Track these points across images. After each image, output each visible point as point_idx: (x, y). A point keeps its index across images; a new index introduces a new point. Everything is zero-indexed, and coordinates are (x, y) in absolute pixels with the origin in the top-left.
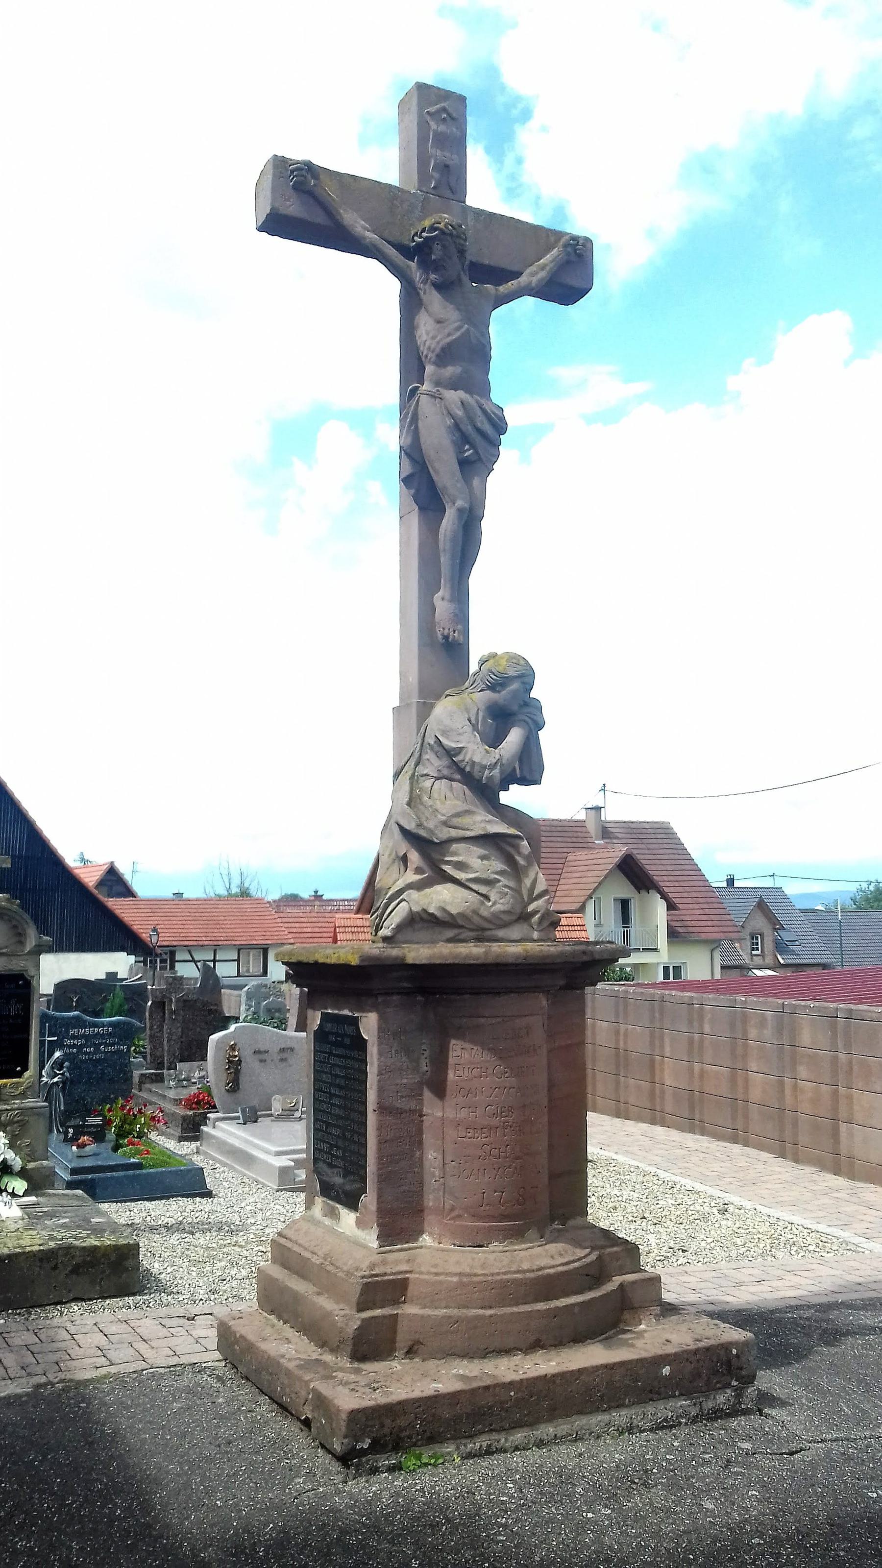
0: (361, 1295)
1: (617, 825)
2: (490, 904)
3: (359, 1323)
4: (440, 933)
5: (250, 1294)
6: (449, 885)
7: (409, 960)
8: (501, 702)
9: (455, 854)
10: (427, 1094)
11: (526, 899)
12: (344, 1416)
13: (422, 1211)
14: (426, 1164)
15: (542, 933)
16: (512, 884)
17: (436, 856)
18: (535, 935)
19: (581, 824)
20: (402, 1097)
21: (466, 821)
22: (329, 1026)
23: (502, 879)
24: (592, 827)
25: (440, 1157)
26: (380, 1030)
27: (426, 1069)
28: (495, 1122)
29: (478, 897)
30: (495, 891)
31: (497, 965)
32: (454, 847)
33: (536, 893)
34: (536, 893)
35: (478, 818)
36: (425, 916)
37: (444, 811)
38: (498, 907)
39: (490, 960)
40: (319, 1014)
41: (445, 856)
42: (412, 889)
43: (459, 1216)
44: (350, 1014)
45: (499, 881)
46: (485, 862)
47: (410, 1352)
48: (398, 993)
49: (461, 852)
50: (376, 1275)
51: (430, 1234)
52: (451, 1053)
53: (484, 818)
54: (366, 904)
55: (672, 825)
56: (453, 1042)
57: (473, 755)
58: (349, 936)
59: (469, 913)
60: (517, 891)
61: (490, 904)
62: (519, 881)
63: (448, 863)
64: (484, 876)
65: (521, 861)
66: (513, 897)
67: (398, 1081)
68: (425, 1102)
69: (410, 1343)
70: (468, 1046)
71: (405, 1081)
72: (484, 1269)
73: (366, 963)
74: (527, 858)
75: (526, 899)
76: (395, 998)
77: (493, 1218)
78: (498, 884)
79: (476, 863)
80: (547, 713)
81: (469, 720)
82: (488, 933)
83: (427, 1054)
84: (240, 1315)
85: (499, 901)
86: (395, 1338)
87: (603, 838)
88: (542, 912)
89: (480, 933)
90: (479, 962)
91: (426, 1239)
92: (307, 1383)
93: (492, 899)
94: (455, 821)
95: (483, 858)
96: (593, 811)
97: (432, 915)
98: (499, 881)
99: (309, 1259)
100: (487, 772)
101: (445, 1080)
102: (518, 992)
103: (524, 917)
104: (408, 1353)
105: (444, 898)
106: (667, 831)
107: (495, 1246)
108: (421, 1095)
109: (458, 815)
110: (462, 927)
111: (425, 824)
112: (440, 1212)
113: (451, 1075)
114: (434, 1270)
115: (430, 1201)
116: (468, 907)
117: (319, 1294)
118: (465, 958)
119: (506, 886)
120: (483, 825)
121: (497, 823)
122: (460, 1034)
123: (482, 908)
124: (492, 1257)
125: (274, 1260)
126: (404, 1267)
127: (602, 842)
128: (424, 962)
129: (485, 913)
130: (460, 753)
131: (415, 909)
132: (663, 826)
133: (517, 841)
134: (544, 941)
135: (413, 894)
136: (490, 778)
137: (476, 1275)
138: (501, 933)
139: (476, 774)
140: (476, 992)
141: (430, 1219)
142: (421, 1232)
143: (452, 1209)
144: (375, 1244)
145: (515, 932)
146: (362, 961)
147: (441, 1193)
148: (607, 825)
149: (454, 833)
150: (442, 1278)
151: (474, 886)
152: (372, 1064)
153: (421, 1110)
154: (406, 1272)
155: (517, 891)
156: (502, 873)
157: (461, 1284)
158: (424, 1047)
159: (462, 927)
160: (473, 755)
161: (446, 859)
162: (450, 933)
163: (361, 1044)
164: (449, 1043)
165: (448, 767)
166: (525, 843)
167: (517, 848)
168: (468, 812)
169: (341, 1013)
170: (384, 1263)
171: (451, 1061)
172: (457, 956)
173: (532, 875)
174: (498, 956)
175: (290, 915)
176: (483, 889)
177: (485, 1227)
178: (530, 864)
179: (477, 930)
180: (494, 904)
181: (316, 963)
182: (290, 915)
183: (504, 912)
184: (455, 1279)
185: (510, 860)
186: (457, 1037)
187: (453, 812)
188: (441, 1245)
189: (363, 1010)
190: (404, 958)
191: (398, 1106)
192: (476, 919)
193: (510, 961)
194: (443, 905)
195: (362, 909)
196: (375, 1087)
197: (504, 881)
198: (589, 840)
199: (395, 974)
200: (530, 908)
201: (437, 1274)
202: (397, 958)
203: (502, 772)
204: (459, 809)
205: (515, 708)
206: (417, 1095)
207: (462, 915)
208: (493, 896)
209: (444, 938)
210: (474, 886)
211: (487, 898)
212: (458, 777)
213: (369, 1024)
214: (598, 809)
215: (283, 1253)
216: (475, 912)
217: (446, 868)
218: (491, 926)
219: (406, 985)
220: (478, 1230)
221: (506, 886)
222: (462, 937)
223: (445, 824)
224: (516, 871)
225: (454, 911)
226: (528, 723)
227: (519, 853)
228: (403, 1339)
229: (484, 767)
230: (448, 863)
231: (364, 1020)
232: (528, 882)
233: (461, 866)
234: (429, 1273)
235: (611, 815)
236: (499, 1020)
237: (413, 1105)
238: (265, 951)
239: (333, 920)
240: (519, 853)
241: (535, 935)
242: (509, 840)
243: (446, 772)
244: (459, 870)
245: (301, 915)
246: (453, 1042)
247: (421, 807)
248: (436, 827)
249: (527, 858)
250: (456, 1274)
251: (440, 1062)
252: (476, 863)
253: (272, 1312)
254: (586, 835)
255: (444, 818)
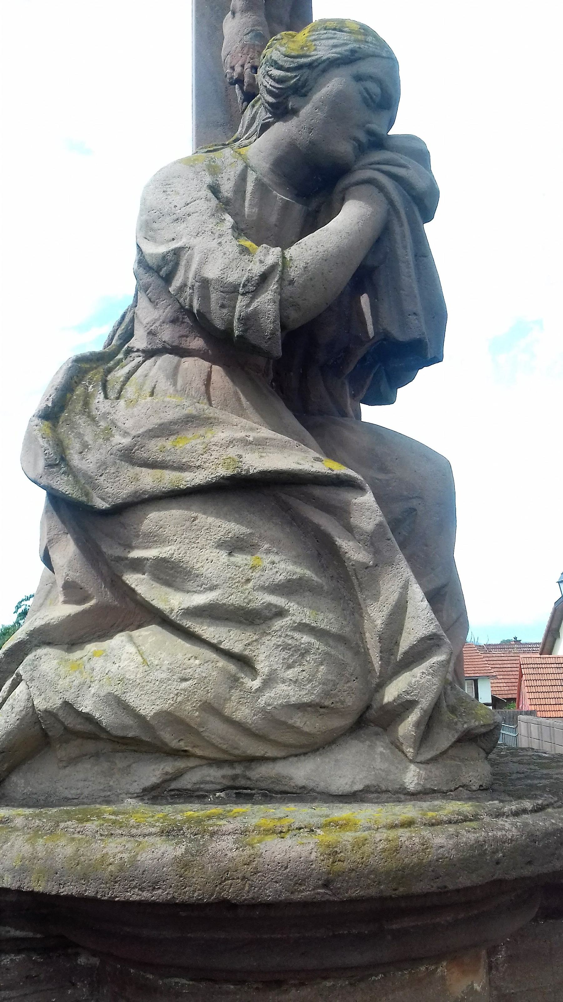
2: (256, 684)
4: (126, 771)
6: (154, 628)
8: (303, 138)
9: (153, 539)
11: (377, 663)
15: (436, 771)
16: (326, 620)
17: (111, 550)
18: (412, 777)
21: (187, 444)
23: (292, 606)
29: (222, 663)
30: (270, 641)
32: (154, 518)
33: (406, 642)
34: (406, 642)
35: (221, 435)
36: (71, 722)
37: (129, 424)
38: (283, 693)
39: (196, 890)
41: (130, 547)
42: (49, 644)
45: (281, 613)
46: (239, 558)
49: (168, 532)
53: (240, 435)
54: (547, 647)
57: (204, 262)
58: (531, 671)
59: (190, 711)
60: (349, 641)
61: (256, 684)
62: (353, 610)
63: (137, 565)
64: (235, 599)
65: (354, 552)
66: (326, 658)
74: (373, 541)
75: (377, 663)
78: (278, 624)
79: (210, 561)
80: (444, 171)
81: (215, 190)
85: (284, 675)
88: (425, 703)
89: (238, 770)
90: (159, 895)
93: (263, 667)
94: (155, 448)
95: (234, 546)
97: (88, 718)
98: (281, 613)
100: (241, 302)
103: (371, 720)
105: (135, 671)
109: (165, 430)
110: (183, 754)
111: (76, 460)
116: (189, 694)
119: (302, 628)
120: (232, 452)
121: (283, 447)
123: (236, 694)
129: (243, 713)
130: (177, 265)
131: (40, 704)
133: (346, 495)
134: (444, 794)
135: (47, 662)
136: (249, 320)
138: (301, 772)
139: (218, 317)
145: (346, 767)
149: (149, 480)
151: (208, 631)
155: (349, 641)
156: (289, 588)
159: (183, 754)
160: (204, 262)
161: (136, 554)
162: (151, 773)
165: (174, 321)
166: (368, 499)
167: (341, 513)
168: (191, 421)
173: (389, 590)
174: (225, 875)
175: (494, 655)
176: (233, 638)
178: (381, 562)
179: (231, 763)
180: (269, 682)
182: (494, 655)
183: (301, 707)
185: (324, 553)
187: (154, 421)
192: (215, 729)
193: (269, 894)
194: (117, 690)
195: (545, 650)
197: (298, 611)
200: (391, 693)
203: (283, 304)
204: (171, 415)
205: (344, 148)
207: (170, 718)
208: (266, 658)
209: (136, 788)
210: (208, 631)
211: (245, 662)
212: (197, 343)
216: (211, 708)
217: (133, 579)
218: (271, 752)
221: (302, 628)
222: (188, 781)
223: (128, 456)
224: (342, 583)
225: (147, 707)
226: (381, 189)
227: (350, 529)
229: (232, 291)
230: (137, 565)
232: (377, 615)
233: (170, 573)
238: (476, 681)
239: (517, 658)
240: (350, 529)
241: (412, 777)
242: (318, 492)
243: (167, 335)
244: (168, 584)
245: (502, 655)
247: (81, 421)
248: (103, 465)
249: (373, 541)
252: (210, 561)
255: (126, 441)
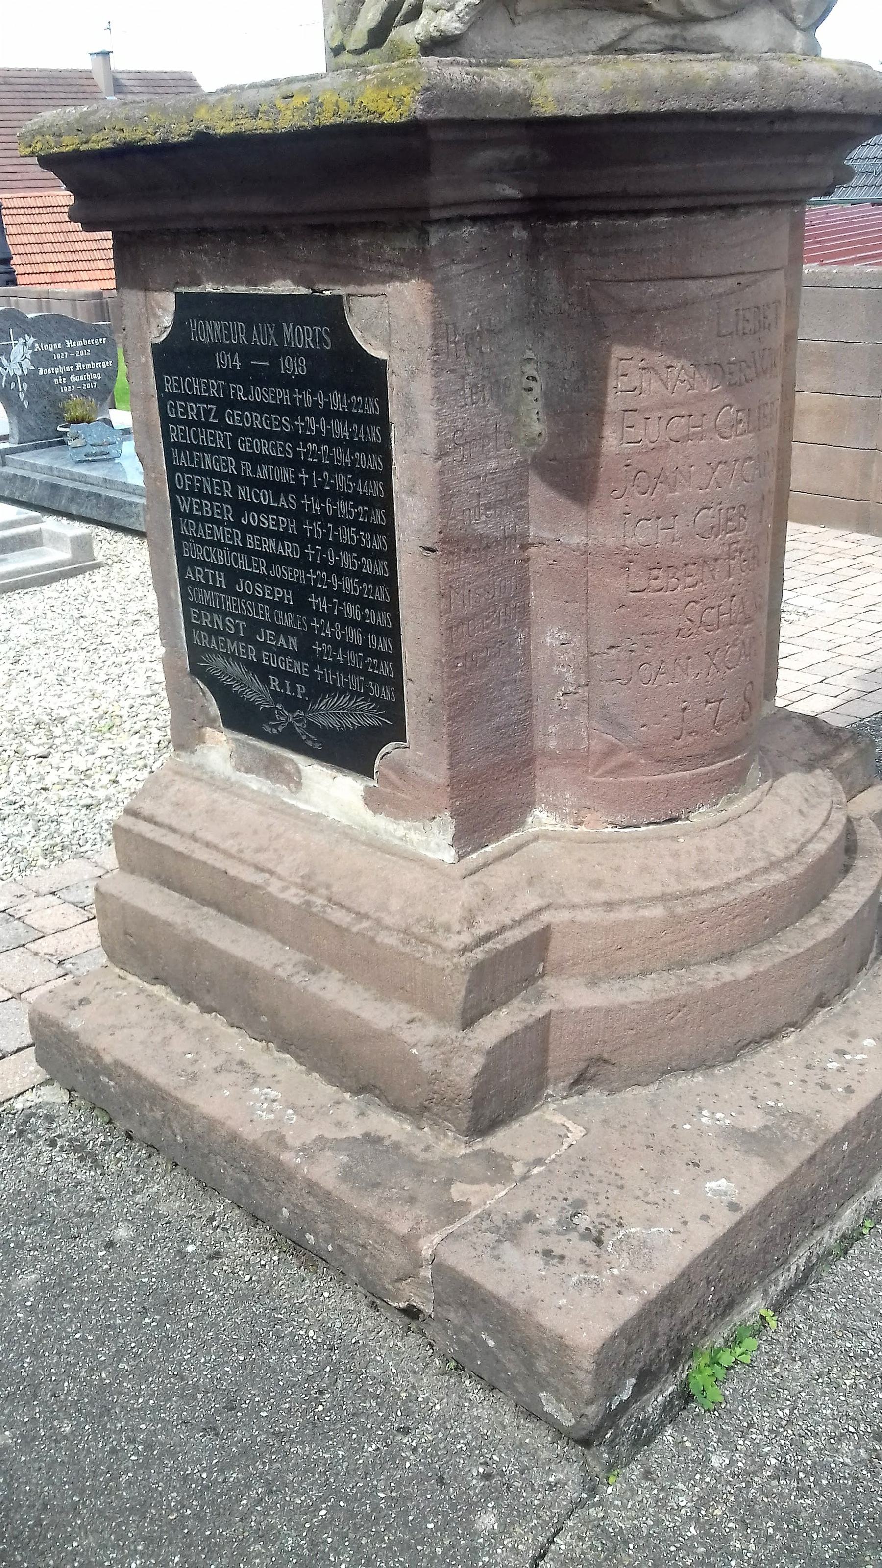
0: (469, 991)
1: (131, 76)
3: (479, 1061)
4: (583, 27)
5: (86, 939)
7: (547, 106)
10: (539, 491)
12: (588, 1364)
13: (529, 762)
14: (540, 657)
19: (87, 75)
20: (488, 507)
22: (208, 332)
24: (101, 80)
25: (578, 640)
26: (441, 329)
27: (537, 428)
28: (714, 546)
31: (788, 115)
40: (168, 301)
43: (626, 766)
44: (303, 291)
47: (580, 1081)
48: (475, 219)
50: (488, 937)
51: (553, 808)
52: (612, 382)
55: (195, 75)
56: (618, 351)
67: (478, 468)
68: (533, 515)
69: (582, 1065)
70: (658, 359)
71: (492, 464)
72: (706, 875)
73: (442, 113)
76: (467, 231)
77: (702, 759)
82: (697, 31)
83: (538, 388)
84: (78, 993)
86: (545, 1060)
87: (116, 92)
91: (541, 819)
92: (407, 1242)
96: (100, 57)
99: (256, 887)
101: (595, 453)
102: (768, 204)
104: (576, 1083)
106: (191, 83)
107: (702, 816)
108: (524, 495)
112: (572, 758)
113: (612, 441)
114: (600, 896)
115: (549, 737)
117: (314, 970)
118: (713, 93)
122: (640, 326)
124: (710, 841)
125: (128, 865)
126: (530, 901)
127: (114, 98)
128: (596, 107)
132: (185, 76)
137: (698, 893)
140: (691, 205)
141: (546, 777)
142: (528, 806)
143: (612, 751)
144: (449, 855)
146: (428, 104)
147: (582, 719)
148: (119, 76)
150: (625, 913)
152: (410, 428)
153: (525, 535)
154: (540, 911)
157: (675, 921)
158: (530, 370)
163: (370, 377)
164: (608, 351)
169: (262, 289)
170: (487, 899)
171: (613, 402)
172: (689, 87)
174: (791, 87)
177: (684, 781)
181: (203, 142)
184: (658, 912)
186: (628, 342)
188: (582, 828)
189: (353, 274)
190: (527, 102)
191: (480, 529)
196: (429, 484)
198: (99, 95)
199: (486, 156)
201: (610, 905)
202: (512, 97)
206: (513, 497)
213: (392, 317)
214: (106, 54)
215: (143, 851)
219: (509, 191)
220: (670, 789)
228: (563, 1056)
231: (357, 304)
234: (589, 905)
235: (118, 63)
236: (731, 282)
237: (510, 524)
246: (618, 351)
250: (653, 900)
251: (579, 408)
253: (157, 979)
254: (94, 89)
